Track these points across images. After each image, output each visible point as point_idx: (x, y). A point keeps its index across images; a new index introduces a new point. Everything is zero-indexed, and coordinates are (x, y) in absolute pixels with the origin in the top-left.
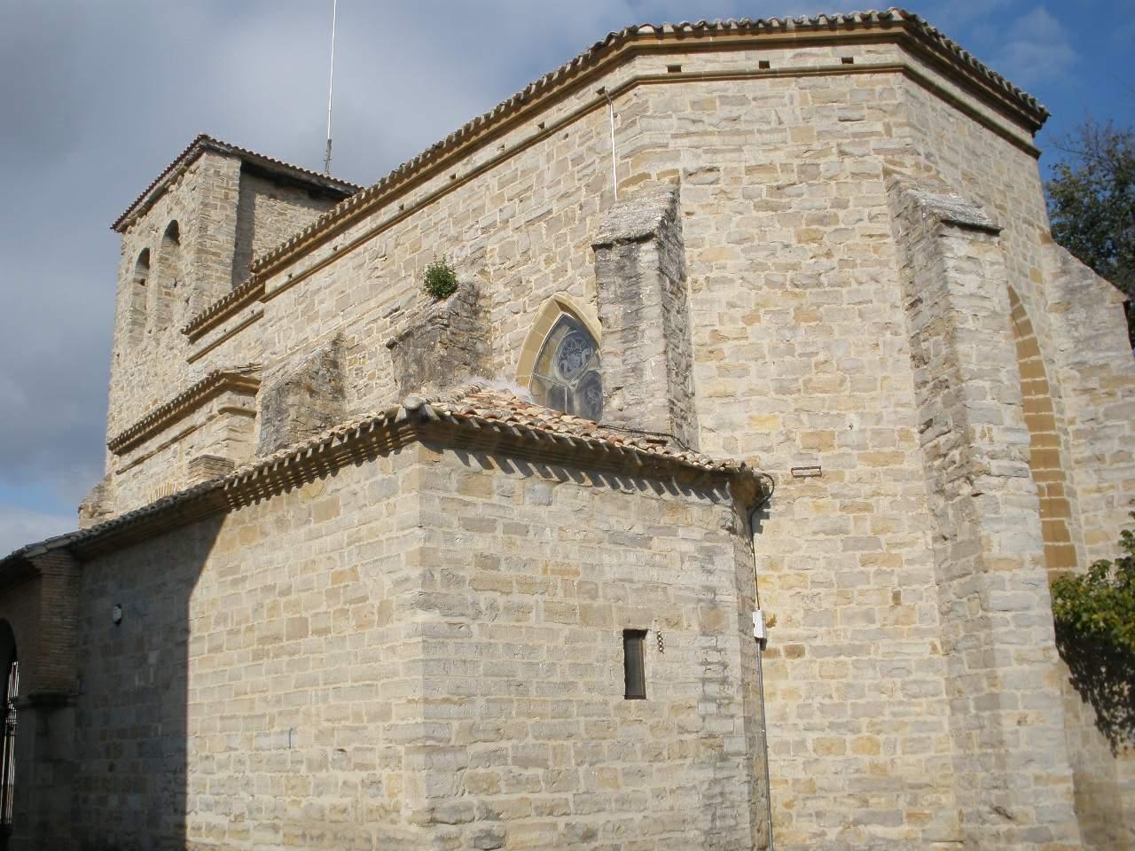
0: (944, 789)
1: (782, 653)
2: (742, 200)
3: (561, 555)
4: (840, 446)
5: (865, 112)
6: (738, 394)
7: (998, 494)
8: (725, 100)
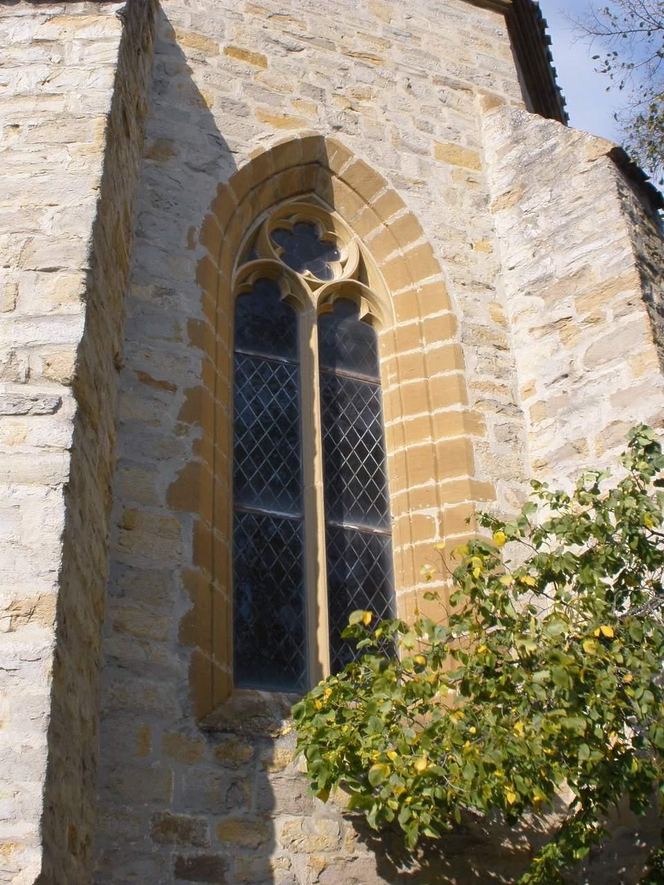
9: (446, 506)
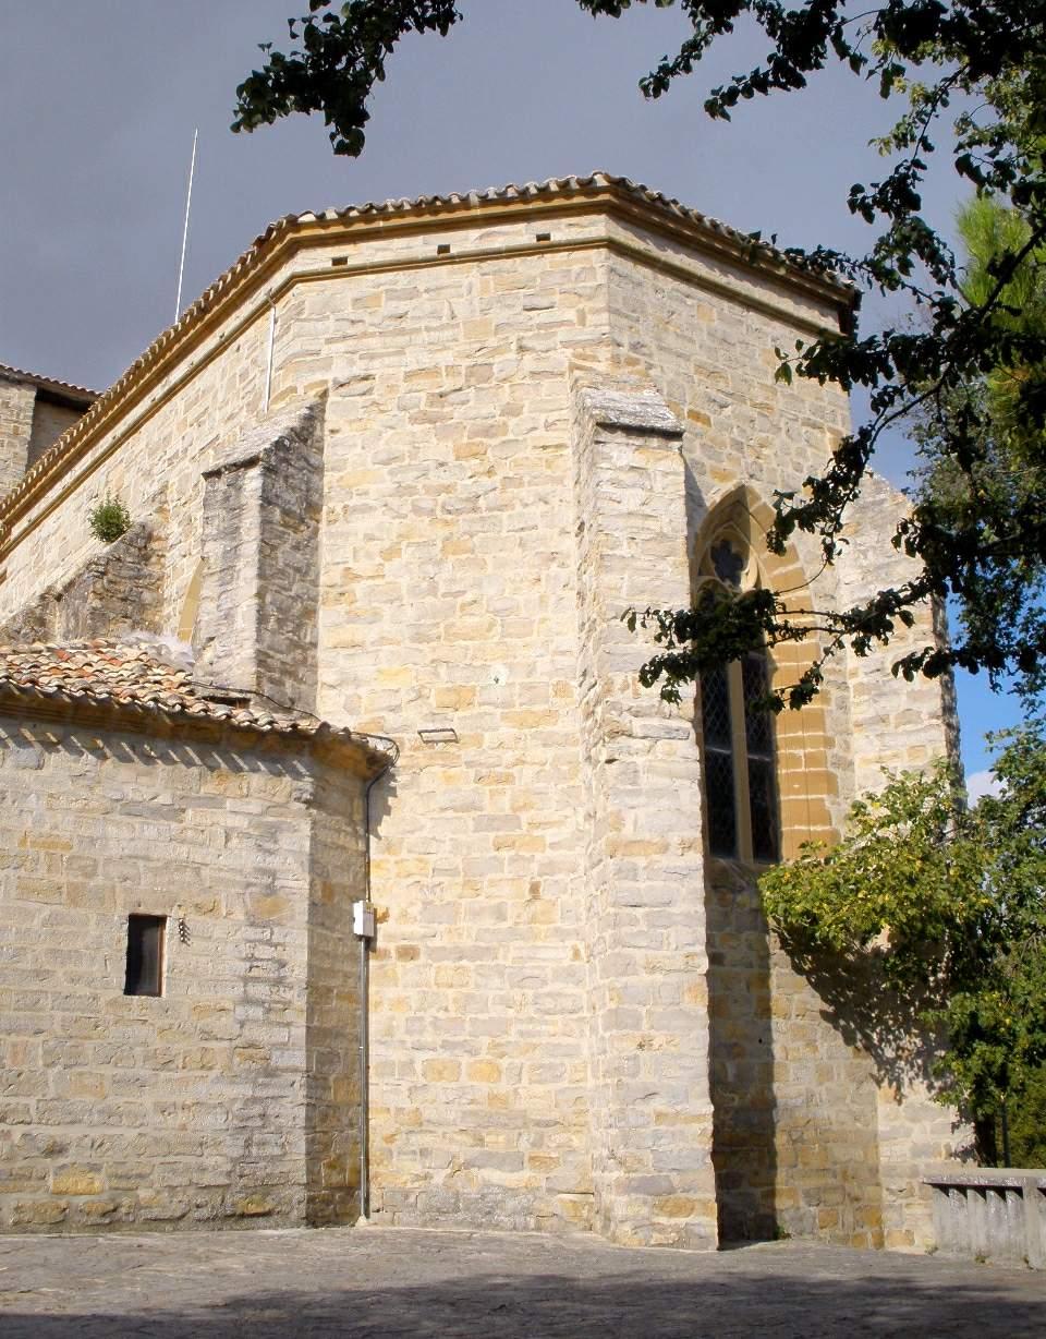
0: (577, 1128)
1: (393, 954)
2: (396, 412)
3: (47, 826)
4: (481, 704)
5: (557, 298)
6: (368, 643)
7: (640, 760)
8: (393, 295)
9: (809, 750)
